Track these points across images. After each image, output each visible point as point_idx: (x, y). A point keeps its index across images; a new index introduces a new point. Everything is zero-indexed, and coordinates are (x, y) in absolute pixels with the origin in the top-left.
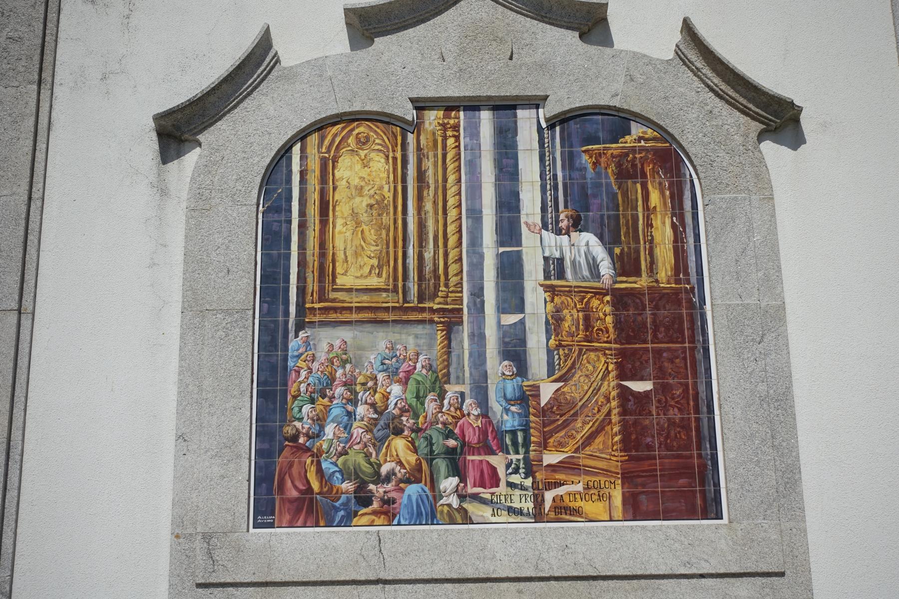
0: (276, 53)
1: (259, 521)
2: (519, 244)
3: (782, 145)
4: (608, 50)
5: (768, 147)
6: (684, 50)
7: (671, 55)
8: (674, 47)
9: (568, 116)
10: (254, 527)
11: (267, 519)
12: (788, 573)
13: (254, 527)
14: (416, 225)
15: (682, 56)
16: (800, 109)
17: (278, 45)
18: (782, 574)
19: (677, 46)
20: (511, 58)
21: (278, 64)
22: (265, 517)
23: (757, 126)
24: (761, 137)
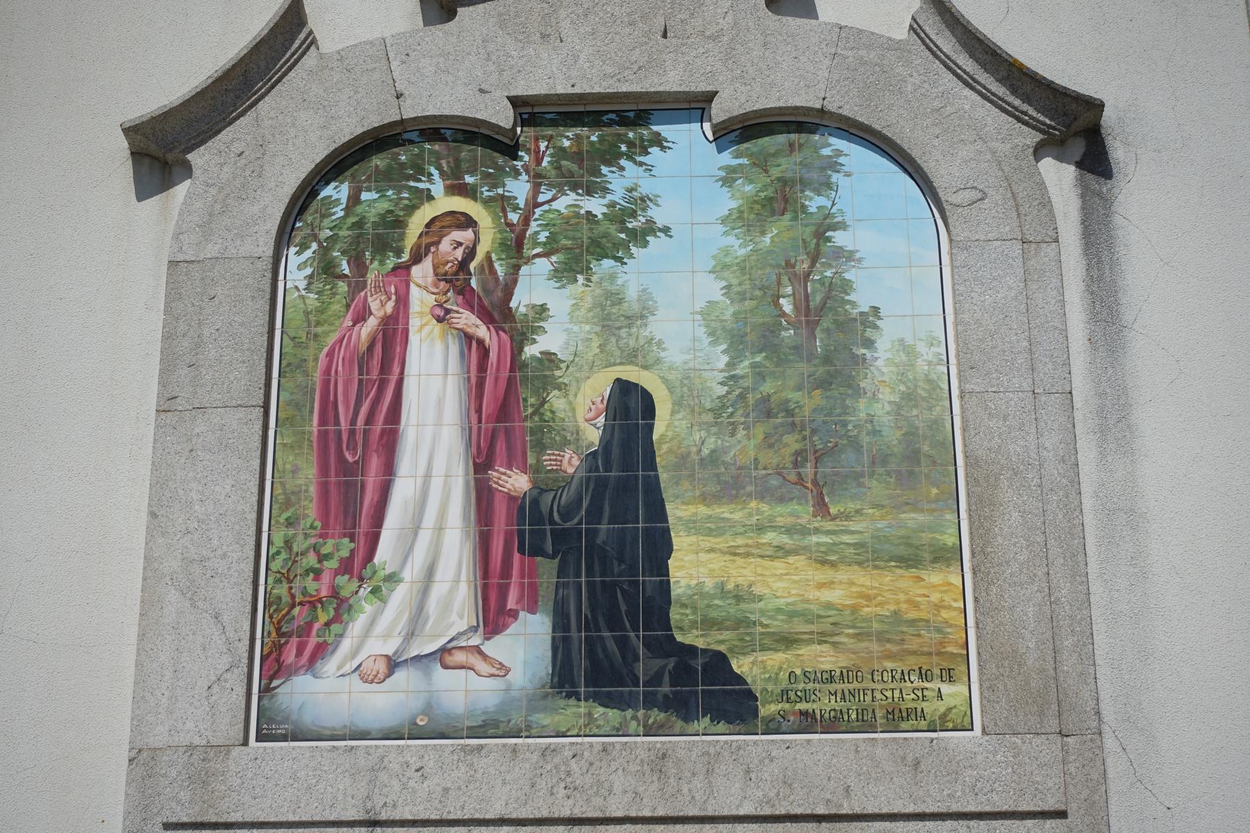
0: (311, 32)
1: (265, 731)
2: (475, 478)
3: (1062, 162)
4: (813, 21)
5: (1048, 165)
6: (933, 37)
7: (901, 33)
8: (909, 20)
9: (967, 63)
10: (257, 740)
11: (276, 729)
12: (1072, 809)
13: (257, 740)
14: (972, 55)
15: (932, 45)
16: (1096, 106)
17: (316, 21)
18: (1062, 814)
19: (914, 19)
20: (665, 36)
21: (313, 48)
22: (274, 727)
23: (1034, 137)
24: (1039, 151)
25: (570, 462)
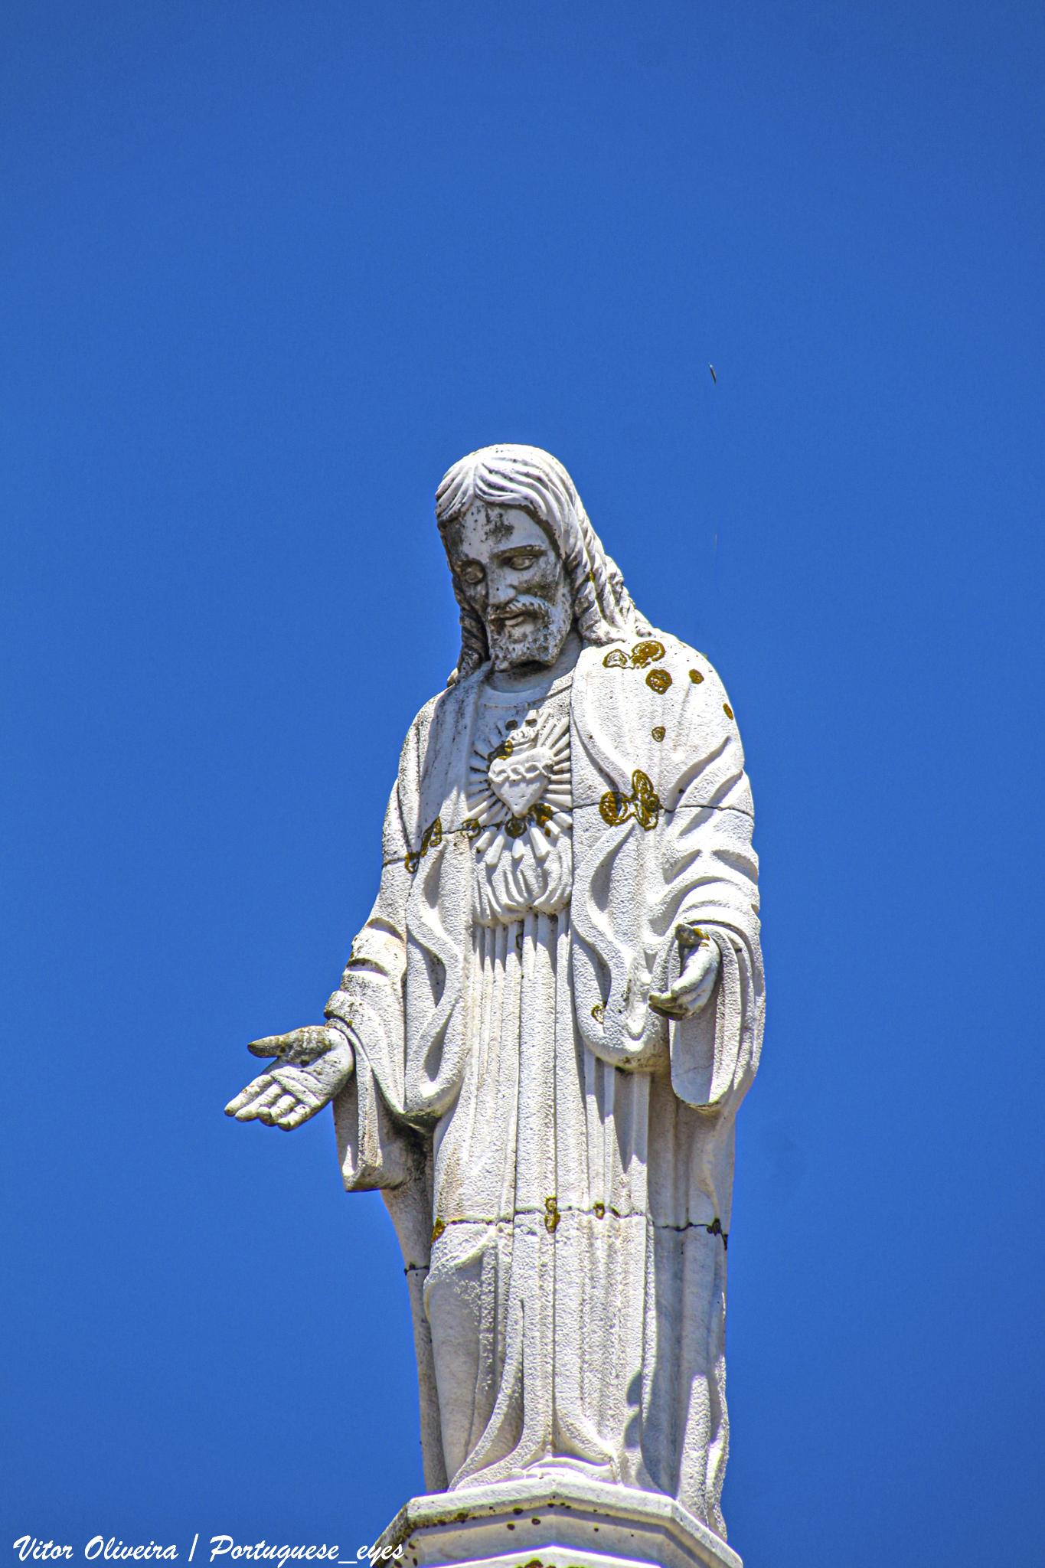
25: (487, 1388)
